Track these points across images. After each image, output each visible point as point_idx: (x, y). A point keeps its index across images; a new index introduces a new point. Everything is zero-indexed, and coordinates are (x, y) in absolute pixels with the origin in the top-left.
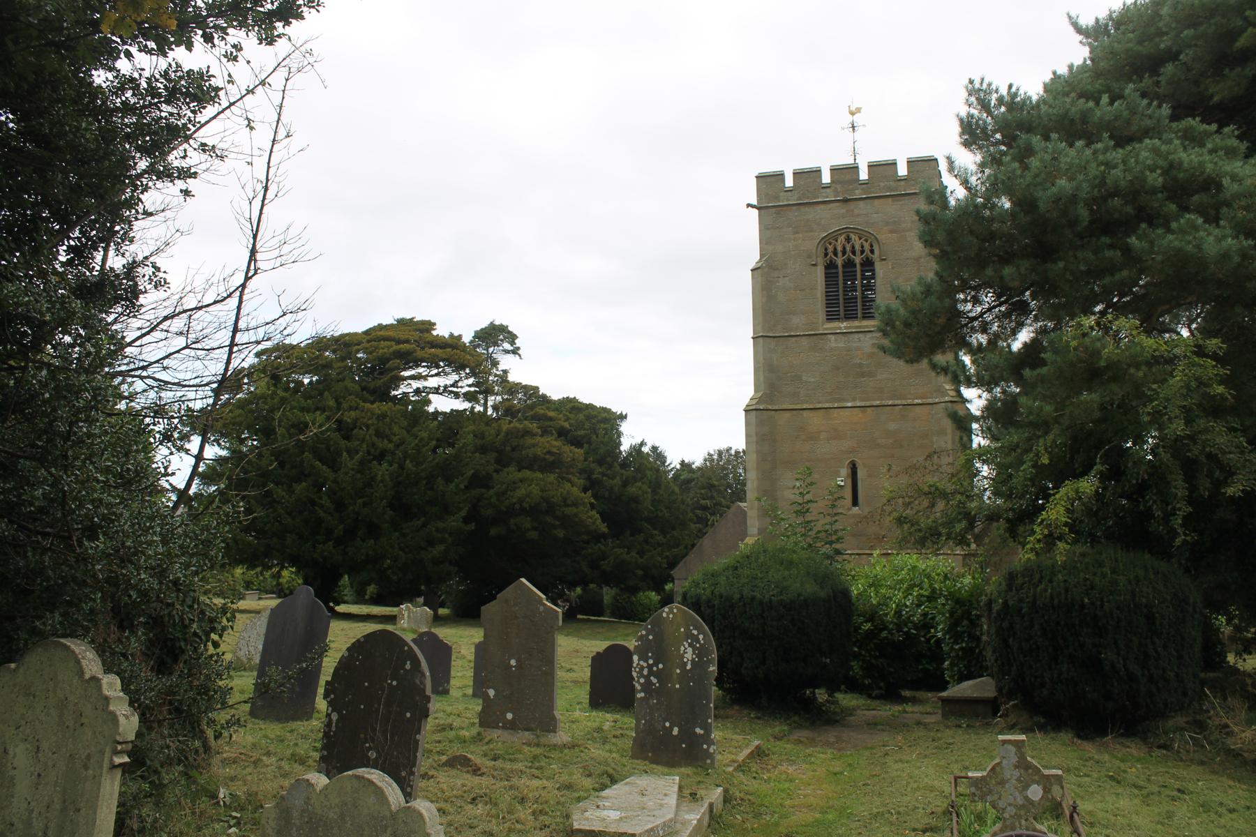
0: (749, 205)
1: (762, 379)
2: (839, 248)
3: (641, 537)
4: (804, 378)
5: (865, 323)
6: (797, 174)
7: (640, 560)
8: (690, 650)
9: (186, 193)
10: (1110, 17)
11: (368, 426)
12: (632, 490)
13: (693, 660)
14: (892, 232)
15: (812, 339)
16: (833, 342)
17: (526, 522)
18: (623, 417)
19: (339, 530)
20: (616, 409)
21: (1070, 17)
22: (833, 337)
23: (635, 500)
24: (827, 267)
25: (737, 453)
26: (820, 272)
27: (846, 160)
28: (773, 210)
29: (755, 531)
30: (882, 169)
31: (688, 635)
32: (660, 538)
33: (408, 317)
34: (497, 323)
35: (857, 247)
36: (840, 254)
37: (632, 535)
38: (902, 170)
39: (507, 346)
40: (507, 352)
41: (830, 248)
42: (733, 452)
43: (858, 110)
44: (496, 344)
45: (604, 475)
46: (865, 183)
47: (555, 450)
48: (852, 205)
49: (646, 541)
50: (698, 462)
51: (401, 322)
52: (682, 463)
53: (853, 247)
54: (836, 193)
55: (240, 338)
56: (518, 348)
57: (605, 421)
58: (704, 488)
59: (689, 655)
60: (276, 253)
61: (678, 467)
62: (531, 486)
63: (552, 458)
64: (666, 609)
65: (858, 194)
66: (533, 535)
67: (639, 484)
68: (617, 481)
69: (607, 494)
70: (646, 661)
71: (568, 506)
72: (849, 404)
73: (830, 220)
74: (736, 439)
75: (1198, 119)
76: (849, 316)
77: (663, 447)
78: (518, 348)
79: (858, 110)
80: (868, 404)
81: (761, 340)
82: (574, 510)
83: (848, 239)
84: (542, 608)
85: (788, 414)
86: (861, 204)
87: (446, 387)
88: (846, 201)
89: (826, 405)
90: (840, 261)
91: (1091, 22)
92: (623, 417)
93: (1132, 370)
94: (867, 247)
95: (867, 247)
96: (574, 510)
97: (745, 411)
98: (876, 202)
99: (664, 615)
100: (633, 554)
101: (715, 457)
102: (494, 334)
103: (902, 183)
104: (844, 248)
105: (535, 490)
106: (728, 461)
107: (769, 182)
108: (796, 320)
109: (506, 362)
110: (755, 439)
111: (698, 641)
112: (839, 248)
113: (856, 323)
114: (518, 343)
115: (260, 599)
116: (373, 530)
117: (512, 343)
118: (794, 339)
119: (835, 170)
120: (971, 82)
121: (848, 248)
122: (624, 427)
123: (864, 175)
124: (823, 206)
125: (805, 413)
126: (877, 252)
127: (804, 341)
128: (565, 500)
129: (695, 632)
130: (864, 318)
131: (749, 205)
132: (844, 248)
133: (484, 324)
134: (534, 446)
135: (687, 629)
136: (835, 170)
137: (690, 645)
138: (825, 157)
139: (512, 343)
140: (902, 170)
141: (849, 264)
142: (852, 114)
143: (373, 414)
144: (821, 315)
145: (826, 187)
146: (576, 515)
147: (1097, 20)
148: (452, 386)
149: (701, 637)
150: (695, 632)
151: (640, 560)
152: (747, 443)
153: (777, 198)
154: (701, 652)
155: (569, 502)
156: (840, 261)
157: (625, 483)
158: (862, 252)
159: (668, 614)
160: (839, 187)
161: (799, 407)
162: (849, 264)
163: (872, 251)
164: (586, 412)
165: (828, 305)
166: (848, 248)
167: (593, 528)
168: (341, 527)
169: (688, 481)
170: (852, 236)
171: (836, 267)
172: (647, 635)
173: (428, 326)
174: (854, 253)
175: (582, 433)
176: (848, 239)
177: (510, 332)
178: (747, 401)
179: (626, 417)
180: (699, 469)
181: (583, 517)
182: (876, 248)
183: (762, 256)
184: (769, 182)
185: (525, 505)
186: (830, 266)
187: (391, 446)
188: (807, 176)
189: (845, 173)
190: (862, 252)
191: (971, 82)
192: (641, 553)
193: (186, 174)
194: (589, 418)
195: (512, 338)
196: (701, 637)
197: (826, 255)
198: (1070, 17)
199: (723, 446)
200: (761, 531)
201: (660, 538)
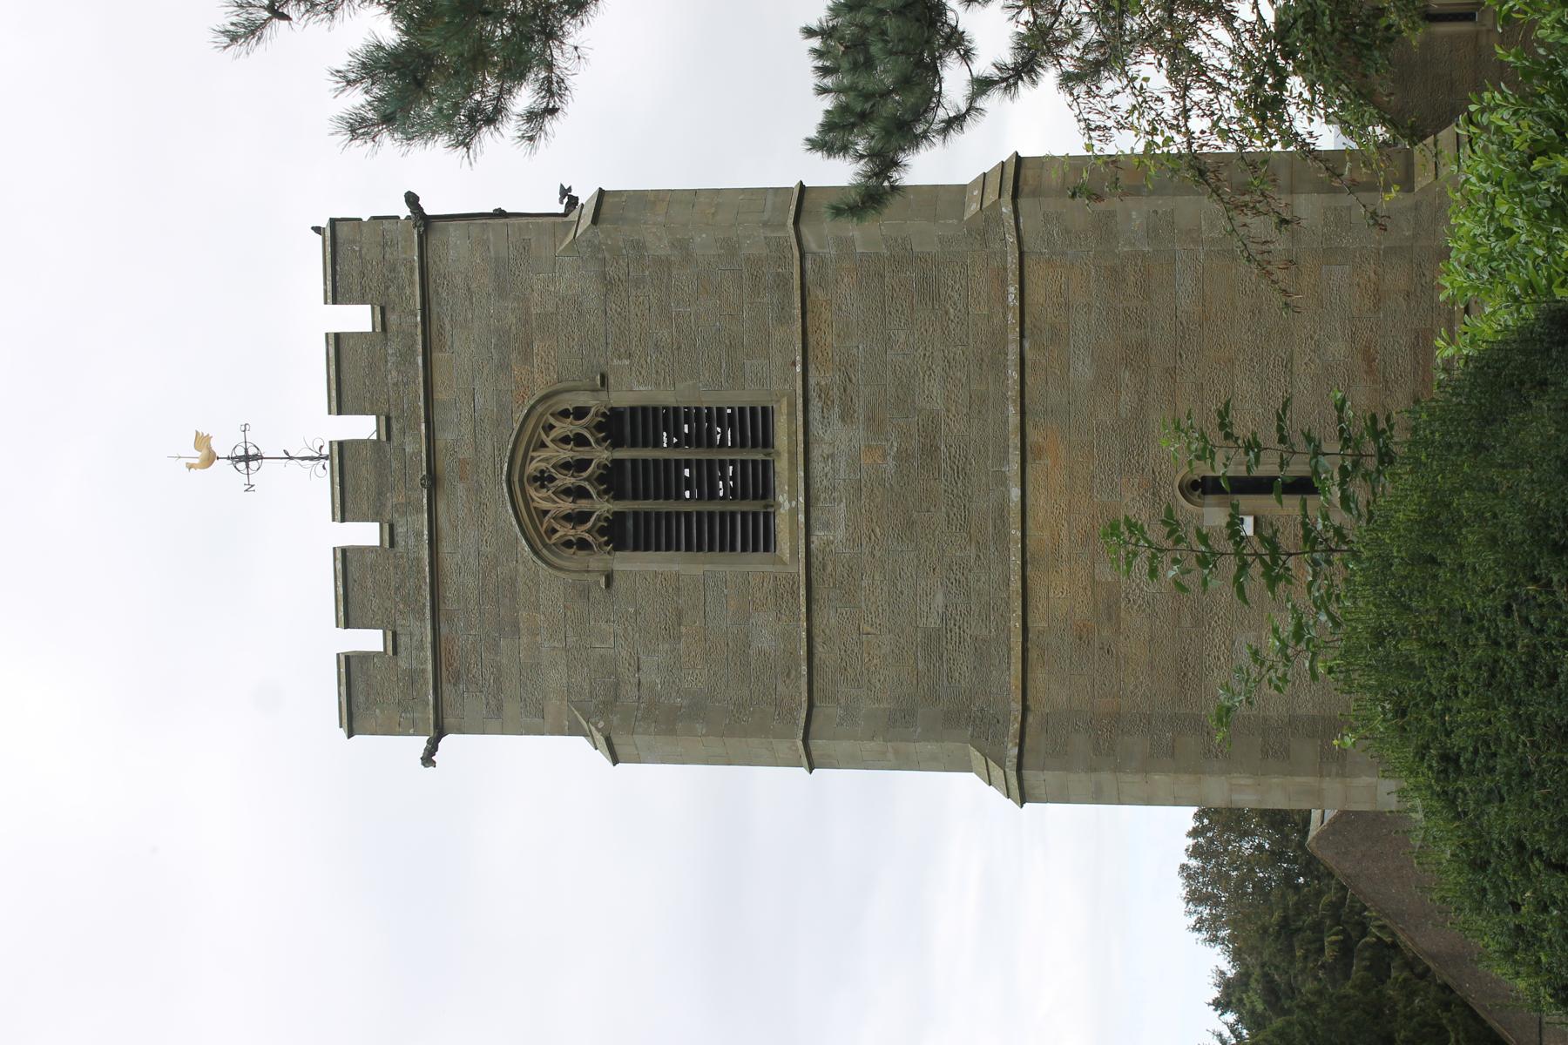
1: (931, 747)
4: (933, 622)
15: (820, 592)
50: (1216, 960)
52: (1221, 1005)
58: (1291, 949)
85: (1038, 675)
106: (1220, 878)
110: (1106, 777)
118: (819, 649)
125: (1037, 623)
127: (827, 618)
169: (1272, 993)
178: (994, 796)
180: (1237, 956)
199: (1179, 888)
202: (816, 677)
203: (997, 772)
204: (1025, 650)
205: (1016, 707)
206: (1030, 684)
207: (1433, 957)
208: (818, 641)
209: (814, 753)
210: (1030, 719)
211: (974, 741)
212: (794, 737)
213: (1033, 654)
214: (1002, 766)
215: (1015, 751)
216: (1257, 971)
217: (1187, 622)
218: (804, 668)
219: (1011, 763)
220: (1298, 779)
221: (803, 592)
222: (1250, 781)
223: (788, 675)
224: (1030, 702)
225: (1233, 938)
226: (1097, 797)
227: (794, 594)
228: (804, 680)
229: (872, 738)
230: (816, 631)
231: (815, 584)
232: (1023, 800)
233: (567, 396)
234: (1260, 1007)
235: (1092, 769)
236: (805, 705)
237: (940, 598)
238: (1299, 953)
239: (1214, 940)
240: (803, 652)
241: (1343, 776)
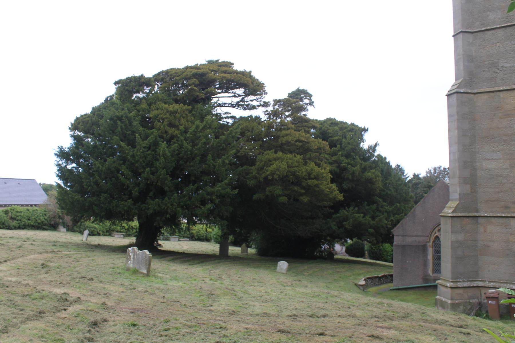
1: (462, 68)
3: (374, 207)
4: (501, 64)
7: (372, 222)
11: (163, 120)
12: (368, 174)
15: (509, 30)
17: (278, 190)
18: (365, 130)
19: (135, 192)
23: (370, 181)
25: (445, 169)
29: (457, 196)
32: (388, 208)
33: (215, 59)
34: (301, 88)
37: (368, 205)
42: (442, 168)
45: (348, 164)
47: (303, 139)
49: (377, 209)
50: (423, 174)
51: (210, 62)
52: (414, 175)
56: (313, 102)
58: (425, 187)
61: (412, 177)
62: (281, 163)
63: (300, 144)
66: (284, 199)
67: (373, 171)
68: (357, 168)
69: (350, 177)
71: (310, 178)
74: (445, 163)
77: (403, 166)
78: (313, 102)
81: (461, 35)
82: (316, 182)
85: (485, 96)
87: (238, 102)
92: (365, 130)
96: (316, 182)
97: (448, 95)
100: (367, 218)
101: (432, 171)
105: (284, 165)
106: (440, 174)
108: (492, 16)
110: (456, 117)
115: (179, 240)
116: (161, 193)
118: (490, 32)
122: (366, 136)
125: (502, 94)
127: (500, 33)
128: (309, 174)
133: (294, 89)
134: (287, 135)
143: (168, 111)
146: (317, 186)
148: (240, 101)
151: (372, 222)
152: (450, 161)
155: (312, 176)
157: (364, 170)
161: (496, 89)
164: (340, 126)
167: (331, 196)
168: (137, 189)
169: (416, 184)
173: (229, 65)
175: (336, 138)
177: (308, 93)
178: (449, 88)
179: (367, 130)
180: (424, 177)
181: (323, 187)
185: (276, 176)
187: (177, 132)
192: (373, 218)
194: (341, 129)
199: (437, 166)
200: (462, 196)
201: (388, 208)
202: (481, 33)
203: (455, 87)
204: (493, 92)
205: (475, 91)
206: (483, 94)
207: (414, 211)
208: (493, 31)
209: (458, 36)
210: (472, 95)
211: (464, 80)
212: (462, 28)
213: (492, 94)
214: (457, 88)
215: (462, 91)
216: (421, 181)
217: (505, 138)
218: (484, 29)
219: (459, 90)
220: (458, 171)
221: (509, 24)
222: (456, 158)
223: (482, 25)
224: (477, 95)
225: (427, 176)
226: (450, 116)
227: (508, 22)
228: (480, 29)
229: (463, 51)
230: (496, 30)
231: (511, 28)
232: (447, 95)
233: (452, 321)
234: (414, 182)
235: (458, 113)
236: (472, 31)
237: (509, 65)
238: (425, 189)
239: (427, 173)
240: (489, 28)
241: (459, 183)
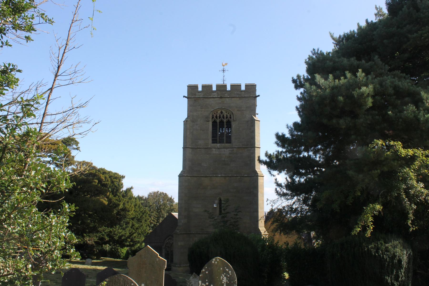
0: (184, 97)
2: (218, 116)
5: (227, 145)
6: (203, 87)
8: (225, 278)
9: (27, 38)
10: (344, 35)
13: (227, 282)
14: (238, 111)
16: (214, 151)
18: (123, 177)
20: (121, 173)
21: (331, 34)
22: (214, 149)
24: (213, 123)
26: (210, 124)
27: (221, 83)
28: (194, 99)
30: (236, 87)
31: (224, 271)
35: (225, 116)
36: (218, 118)
38: (243, 88)
39: (75, 146)
40: (74, 149)
41: (215, 115)
43: (226, 64)
44: (69, 145)
46: (229, 91)
48: (223, 99)
53: (223, 116)
54: (218, 94)
55: (48, 119)
56: (79, 148)
57: (116, 178)
59: (225, 280)
60: (69, 77)
64: (214, 260)
65: (226, 95)
70: (205, 283)
72: (220, 176)
73: (215, 104)
75: (400, 71)
76: (221, 142)
78: (79, 148)
79: (226, 64)
80: (227, 176)
83: (222, 112)
84: (158, 260)
86: (227, 99)
88: (221, 98)
89: (211, 175)
90: (218, 121)
91: (338, 36)
92: (123, 177)
93: (392, 162)
94: (229, 116)
95: (229, 116)
98: (233, 99)
99: (213, 262)
102: (69, 142)
103: (243, 93)
104: (220, 116)
107: (192, 89)
109: (74, 153)
111: (229, 274)
112: (218, 116)
113: (223, 145)
114: (79, 145)
117: (77, 145)
118: (199, 149)
119: (218, 86)
120: (314, 50)
121: (221, 116)
122: (124, 181)
123: (229, 88)
124: (212, 99)
126: (232, 118)
129: (227, 270)
130: (227, 143)
131: (184, 97)
132: (227, 116)
135: (224, 268)
136: (218, 86)
137: (225, 276)
138: (214, 82)
139: (77, 145)
140: (243, 88)
141: (222, 122)
142: (223, 65)
144: (210, 141)
145: (214, 92)
147: (340, 36)
149: (230, 272)
150: (227, 270)
153: (195, 95)
154: (230, 279)
156: (218, 121)
158: (227, 117)
159: (215, 262)
160: (219, 92)
161: (200, 176)
162: (222, 122)
163: (230, 117)
165: (213, 137)
166: (221, 116)
170: (223, 111)
171: (217, 123)
172: (205, 271)
174: (223, 117)
176: (222, 112)
177: (76, 141)
179: (124, 177)
182: (232, 116)
183: (188, 116)
184: (192, 89)
186: (214, 123)
188: (207, 88)
189: (221, 88)
190: (220, 117)
191: (314, 50)
193: (31, 29)
195: (77, 143)
196: (230, 272)
197: (213, 118)
198: (331, 34)
